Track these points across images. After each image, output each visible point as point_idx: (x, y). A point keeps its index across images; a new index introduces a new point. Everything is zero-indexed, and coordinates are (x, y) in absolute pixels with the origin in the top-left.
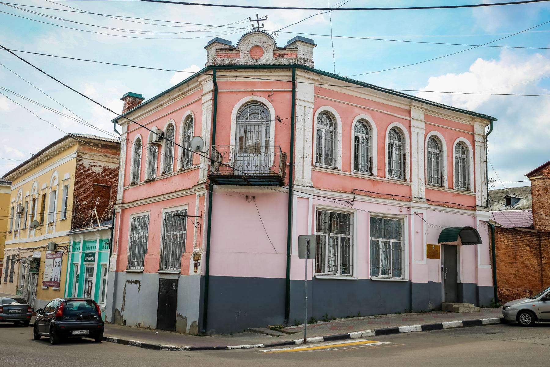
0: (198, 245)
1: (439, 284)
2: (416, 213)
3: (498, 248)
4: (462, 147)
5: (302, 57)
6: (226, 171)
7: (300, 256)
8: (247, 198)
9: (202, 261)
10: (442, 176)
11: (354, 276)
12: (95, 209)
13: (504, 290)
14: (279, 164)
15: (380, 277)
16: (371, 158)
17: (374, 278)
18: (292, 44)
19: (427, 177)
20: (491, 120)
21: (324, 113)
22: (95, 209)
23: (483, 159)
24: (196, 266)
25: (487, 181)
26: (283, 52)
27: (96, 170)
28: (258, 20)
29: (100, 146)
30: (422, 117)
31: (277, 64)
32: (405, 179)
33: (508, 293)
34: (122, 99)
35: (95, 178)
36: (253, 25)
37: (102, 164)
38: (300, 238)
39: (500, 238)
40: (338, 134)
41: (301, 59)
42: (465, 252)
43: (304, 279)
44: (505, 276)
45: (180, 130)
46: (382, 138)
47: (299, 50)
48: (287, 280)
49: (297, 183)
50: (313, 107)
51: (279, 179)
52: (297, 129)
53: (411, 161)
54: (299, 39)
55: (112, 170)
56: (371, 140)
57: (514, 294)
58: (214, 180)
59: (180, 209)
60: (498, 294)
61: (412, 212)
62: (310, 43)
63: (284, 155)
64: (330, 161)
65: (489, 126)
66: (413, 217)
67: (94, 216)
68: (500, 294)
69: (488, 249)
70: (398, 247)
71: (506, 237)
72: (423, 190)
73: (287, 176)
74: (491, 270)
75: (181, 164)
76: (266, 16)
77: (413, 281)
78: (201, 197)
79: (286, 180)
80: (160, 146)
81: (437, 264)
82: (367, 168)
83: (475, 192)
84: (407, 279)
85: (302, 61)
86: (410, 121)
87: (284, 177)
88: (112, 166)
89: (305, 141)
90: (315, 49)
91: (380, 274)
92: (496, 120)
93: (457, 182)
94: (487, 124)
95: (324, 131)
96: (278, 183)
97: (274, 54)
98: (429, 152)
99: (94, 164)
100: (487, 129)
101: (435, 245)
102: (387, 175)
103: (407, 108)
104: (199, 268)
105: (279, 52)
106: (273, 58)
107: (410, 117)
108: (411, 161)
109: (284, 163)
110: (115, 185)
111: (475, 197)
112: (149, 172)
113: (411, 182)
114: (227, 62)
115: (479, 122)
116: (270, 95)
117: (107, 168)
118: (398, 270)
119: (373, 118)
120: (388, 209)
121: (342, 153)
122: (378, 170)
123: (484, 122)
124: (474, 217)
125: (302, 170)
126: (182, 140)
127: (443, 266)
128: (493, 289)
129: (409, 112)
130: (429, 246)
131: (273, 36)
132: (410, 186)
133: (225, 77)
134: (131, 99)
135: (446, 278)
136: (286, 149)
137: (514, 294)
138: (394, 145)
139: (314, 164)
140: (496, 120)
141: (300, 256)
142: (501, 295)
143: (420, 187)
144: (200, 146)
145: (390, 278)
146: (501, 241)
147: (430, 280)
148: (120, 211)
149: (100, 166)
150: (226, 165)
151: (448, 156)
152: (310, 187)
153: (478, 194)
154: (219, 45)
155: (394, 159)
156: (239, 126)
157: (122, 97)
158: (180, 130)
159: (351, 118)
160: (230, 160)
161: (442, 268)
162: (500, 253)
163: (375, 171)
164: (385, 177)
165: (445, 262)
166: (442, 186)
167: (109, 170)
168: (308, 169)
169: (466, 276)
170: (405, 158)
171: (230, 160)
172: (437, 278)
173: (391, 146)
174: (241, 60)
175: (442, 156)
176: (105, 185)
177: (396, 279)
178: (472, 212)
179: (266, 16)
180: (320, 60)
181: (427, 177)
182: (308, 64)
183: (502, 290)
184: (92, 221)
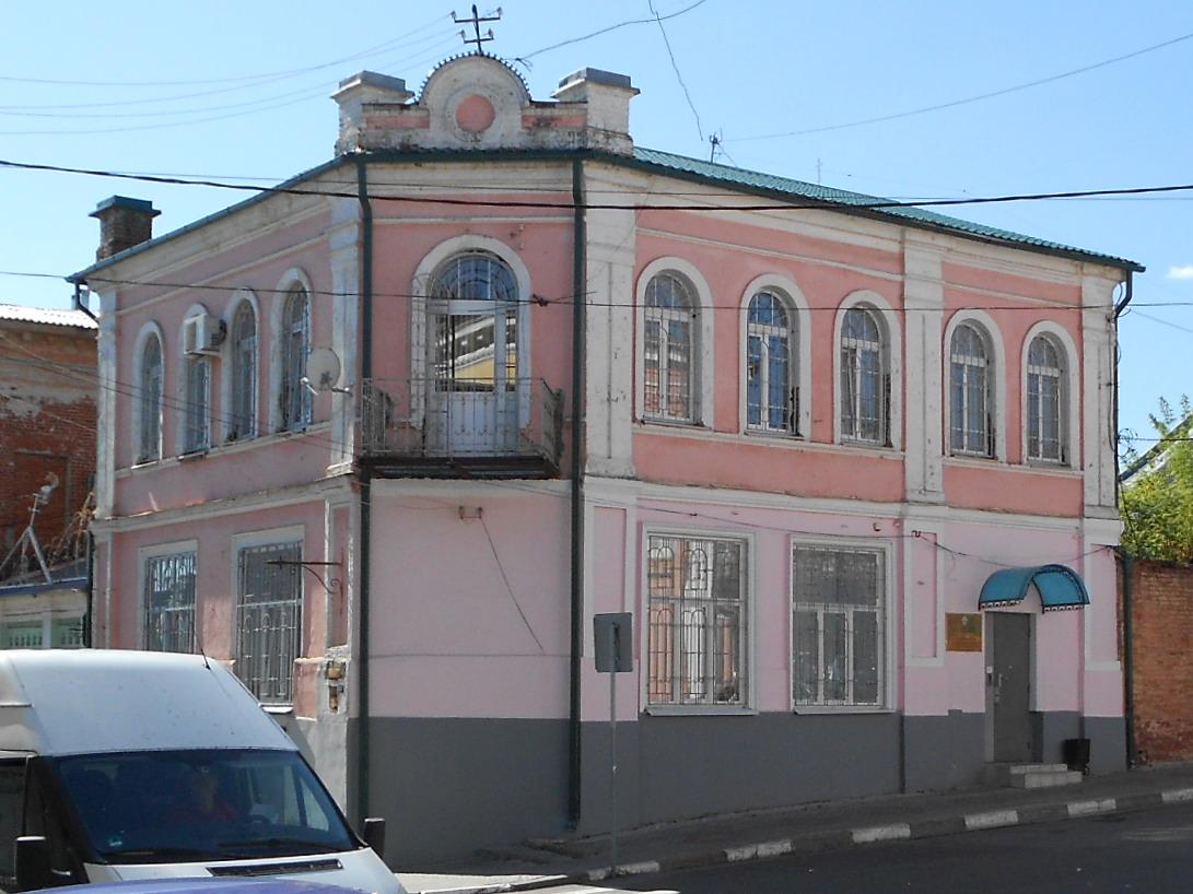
0: (335, 640)
1: (977, 717)
2: (918, 534)
3: (1139, 617)
4: (1048, 350)
5: (601, 126)
6: (402, 443)
7: (599, 668)
8: (461, 512)
9: (350, 682)
10: (991, 430)
11: (751, 704)
12: (29, 530)
13: (1154, 724)
14: (547, 424)
15: (822, 705)
16: (796, 390)
17: (806, 707)
18: (573, 100)
19: (947, 432)
20: (1127, 269)
21: (667, 277)
22: (29, 530)
23: (1107, 377)
24: (334, 694)
25: (1117, 438)
26: (547, 112)
27: (21, 409)
28: (476, 21)
29: (27, 337)
30: (937, 272)
31: (533, 146)
32: (888, 444)
33: (1165, 731)
34: (94, 215)
35: (18, 434)
36: (463, 32)
37: (40, 392)
38: (598, 619)
39: (1148, 588)
40: (705, 334)
41: (596, 131)
42: (1052, 634)
43: (609, 720)
44: (1157, 686)
45: (272, 321)
46: (824, 337)
47: (590, 106)
48: (573, 724)
49: (594, 470)
50: (633, 263)
51: (550, 453)
52: (589, 324)
53: (904, 394)
54: (595, 77)
55: (67, 407)
56: (796, 342)
57: (1179, 735)
58: (369, 467)
59: (283, 536)
60: (1136, 735)
61: (907, 530)
62: (621, 83)
63: (558, 397)
64: (689, 405)
65: (1124, 284)
66: (907, 542)
67: (31, 551)
68: (1141, 735)
69: (1115, 621)
70: (868, 630)
71: (1164, 585)
72: (938, 469)
73: (567, 453)
74: (1120, 676)
75: (280, 417)
76: (499, 10)
77: (910, 711)
78: (340, 516)
79: (565, 463)
80: (215, 360)
81: (975, 665)
82: (785, 420)
83: (1082, 469)
84: (892, 706)
85: (600, 137)
86: (902, 285)
87: (558, 454)
88: (69, 396)
89: (612, 355)
90: (634, 100)
91: (821, 696)
92: (1142, 270)
93: (1033, 445)
94: (1120, 282)
95: (666, 325)
96: (542, 472)
97: (524, 118)
98: (958, 367)
99: (15, 393)
100: (1118, 293)
101: (967, 616)
102: (838, 436)
103: (894, 248)
104: (343, 699)
105: (541, 115)
106: (520, 129)
107: (903, 273)
108: (904, 394)
109: (558, 418)
110: (79, 453)
111: (1082, 481)
112: (189, 433)
113: (903, 450)
114: (396, 140)
115: (1096, 275)
116: (513, 235)
117: (51, 403)
118: (867, 689)
119: (801, 284)
120: (843, 522)
121: (719, 376)
122: (815, 422)
123: (1109, 276)
124: (1080, 538)
125: (605, 433)
126: (278, 350)
127: (990, 670)
128: (1124, 724)
129: (901, 259)
130: (952, 620)
131: (520, 68)
132: (903, 462)
133: (388, 179)
134: (121, 213)
135: (997, 699)
136: (559, 379)
137: (1179, 735)
138: (859, 353)
139: (639, 417)
140: (1142, 270)
141: (599, 668)
142: (1147, 738)
143: (928, 463)
144: (331, 376)
145: (849, 705)
146: (1149, 598)
147: (953, 708)
148: (109, 539)
149: (31, 398)
150: (403, 426)
151: (1009, 375)
152: (629, 478)
153: (1090, 475)
154: (375, 96)
155: (858, 392)
156: (433, 318)
157: (95, 209)
158: (272, 321)
159: (740, 286)
160: (414, 410)
161: (990, 676)
162: (1145, 631)
163: (805, 426)
164: (832, 442)
165: (997, 658)
166: (992, 455)
167: (58, 408)
168: (623, 430)
169: (1052, 694)
170: (889, 385)
171: (414, 410)
172: (974, 700)
173: (849, 354)
174: (434, 137)
175: (992, 374)
176: (48, 452)
177: (863, 707)
178: (1076, 522)
179: (499, 10)
180: (653, 127)
181: (947, 432)
182: (618, 146)
183: (1148, 725)
184: (25, 565)
